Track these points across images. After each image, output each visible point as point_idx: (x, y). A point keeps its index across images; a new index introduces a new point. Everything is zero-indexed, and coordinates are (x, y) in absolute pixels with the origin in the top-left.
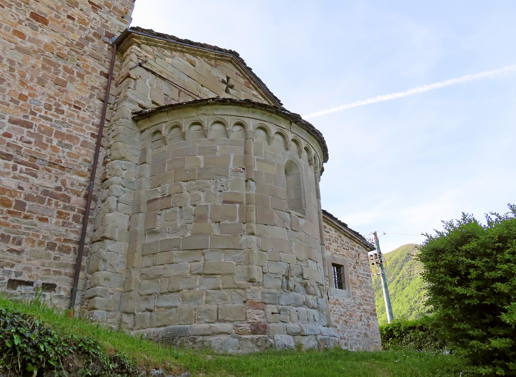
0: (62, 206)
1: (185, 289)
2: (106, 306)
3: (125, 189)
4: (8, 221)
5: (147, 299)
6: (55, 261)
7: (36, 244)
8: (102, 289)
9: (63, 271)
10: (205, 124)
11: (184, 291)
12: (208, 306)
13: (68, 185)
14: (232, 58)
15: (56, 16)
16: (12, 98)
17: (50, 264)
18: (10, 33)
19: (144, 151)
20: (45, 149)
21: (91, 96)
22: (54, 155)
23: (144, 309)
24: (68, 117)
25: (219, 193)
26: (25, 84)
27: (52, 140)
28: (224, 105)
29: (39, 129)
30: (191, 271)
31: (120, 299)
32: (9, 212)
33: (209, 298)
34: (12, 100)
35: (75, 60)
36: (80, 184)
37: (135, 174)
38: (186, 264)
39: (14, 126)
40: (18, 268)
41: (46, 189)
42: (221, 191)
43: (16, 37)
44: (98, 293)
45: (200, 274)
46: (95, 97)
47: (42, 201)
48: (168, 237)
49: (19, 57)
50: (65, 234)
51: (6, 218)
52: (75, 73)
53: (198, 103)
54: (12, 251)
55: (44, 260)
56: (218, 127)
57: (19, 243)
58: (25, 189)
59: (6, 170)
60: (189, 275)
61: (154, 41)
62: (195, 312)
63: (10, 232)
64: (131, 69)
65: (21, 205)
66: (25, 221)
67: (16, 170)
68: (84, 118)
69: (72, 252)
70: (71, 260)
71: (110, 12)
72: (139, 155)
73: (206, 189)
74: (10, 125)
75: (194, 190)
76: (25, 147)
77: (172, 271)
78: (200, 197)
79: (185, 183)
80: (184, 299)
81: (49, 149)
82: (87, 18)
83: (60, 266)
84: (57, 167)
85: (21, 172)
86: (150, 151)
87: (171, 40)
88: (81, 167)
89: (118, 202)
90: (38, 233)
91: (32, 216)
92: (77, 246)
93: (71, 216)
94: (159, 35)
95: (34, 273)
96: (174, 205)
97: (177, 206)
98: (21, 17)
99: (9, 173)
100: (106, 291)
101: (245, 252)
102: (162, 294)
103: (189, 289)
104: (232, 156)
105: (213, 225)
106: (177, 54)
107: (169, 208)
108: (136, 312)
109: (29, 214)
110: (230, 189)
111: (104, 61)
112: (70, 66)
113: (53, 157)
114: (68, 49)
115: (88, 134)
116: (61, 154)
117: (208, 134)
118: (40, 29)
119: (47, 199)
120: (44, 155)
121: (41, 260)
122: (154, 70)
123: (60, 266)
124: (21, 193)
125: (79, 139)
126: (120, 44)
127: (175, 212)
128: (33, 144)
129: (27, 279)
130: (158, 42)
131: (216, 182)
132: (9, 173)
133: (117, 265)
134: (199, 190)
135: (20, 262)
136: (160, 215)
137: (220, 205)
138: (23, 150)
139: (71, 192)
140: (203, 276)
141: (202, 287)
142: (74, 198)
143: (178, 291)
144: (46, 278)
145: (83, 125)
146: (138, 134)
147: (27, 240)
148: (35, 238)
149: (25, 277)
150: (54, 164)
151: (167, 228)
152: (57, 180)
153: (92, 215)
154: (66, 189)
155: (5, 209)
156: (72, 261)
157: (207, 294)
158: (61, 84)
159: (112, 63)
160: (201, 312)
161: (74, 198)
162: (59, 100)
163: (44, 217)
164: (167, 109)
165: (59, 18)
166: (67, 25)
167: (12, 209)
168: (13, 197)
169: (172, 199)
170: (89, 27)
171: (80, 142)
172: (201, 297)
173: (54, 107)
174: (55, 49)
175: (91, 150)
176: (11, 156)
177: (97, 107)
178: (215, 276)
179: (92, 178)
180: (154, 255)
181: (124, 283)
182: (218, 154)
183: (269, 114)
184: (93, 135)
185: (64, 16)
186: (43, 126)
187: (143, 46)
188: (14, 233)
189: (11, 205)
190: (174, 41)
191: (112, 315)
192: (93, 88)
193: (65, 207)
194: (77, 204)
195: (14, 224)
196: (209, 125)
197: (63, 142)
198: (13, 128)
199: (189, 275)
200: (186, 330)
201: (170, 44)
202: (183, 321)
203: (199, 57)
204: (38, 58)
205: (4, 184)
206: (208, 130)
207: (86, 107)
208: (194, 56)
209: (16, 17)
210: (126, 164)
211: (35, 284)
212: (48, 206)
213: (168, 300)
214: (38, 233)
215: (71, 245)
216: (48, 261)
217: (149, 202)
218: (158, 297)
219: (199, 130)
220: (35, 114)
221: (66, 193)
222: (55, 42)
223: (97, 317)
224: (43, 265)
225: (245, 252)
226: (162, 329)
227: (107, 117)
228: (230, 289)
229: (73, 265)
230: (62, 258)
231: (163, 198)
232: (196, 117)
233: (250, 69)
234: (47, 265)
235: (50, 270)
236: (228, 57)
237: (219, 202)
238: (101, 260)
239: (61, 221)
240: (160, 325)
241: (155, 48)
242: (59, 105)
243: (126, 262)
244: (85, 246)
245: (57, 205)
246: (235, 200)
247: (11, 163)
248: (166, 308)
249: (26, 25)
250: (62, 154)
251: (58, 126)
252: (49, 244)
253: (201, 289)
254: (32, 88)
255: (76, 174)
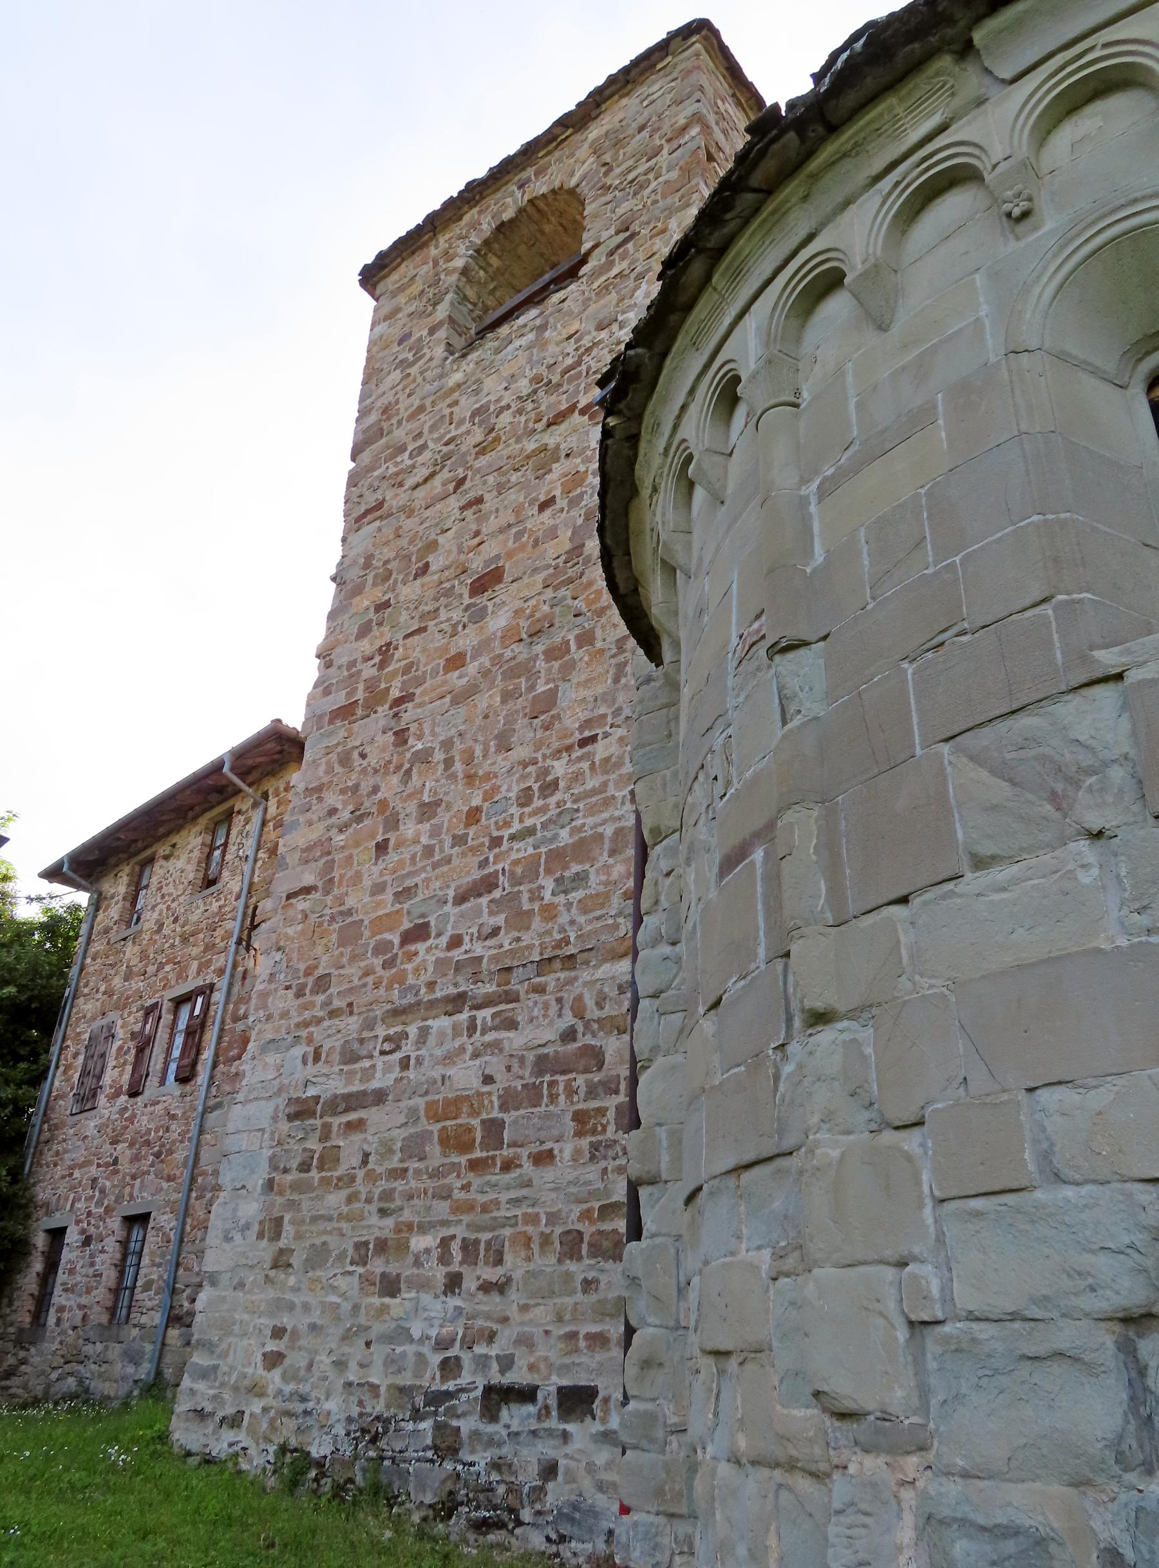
2: (659, 1493)
32: (474, 1165)
50: (600, 1185)
55: (558, 1301)
65: (494, 1128)
115: (623, 803)
121: (551, 1302)
139: (601, 1028)
148: (530, 1229)
149: (518, 1377)
167: (478, 1154)
183: (792, 190)
193: (592, 1093)
216: (569, 1301)
245: (571, 1092)
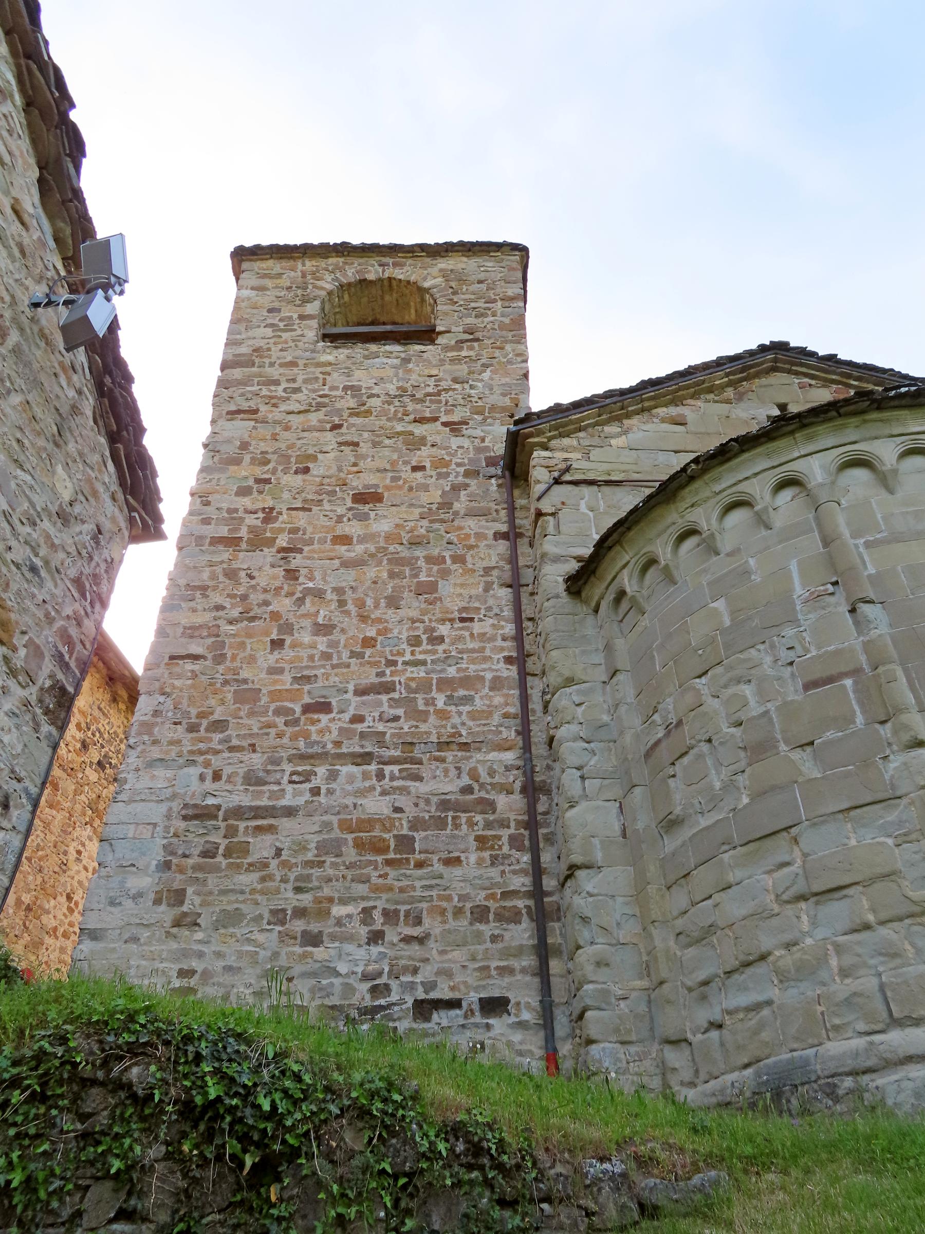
0: (481, 824)
1: (777, 947)
2: (617, 1030)
3: (592, 745)
4: (389, 881)
5: (704, 998)
6: (494, 946)
7: (450, 915)
8: (596, 990)
9: (516, 964)
10: (704, 526)
11: (777, 953)
12: (852, 985)
13: (484, 777)
14: (775, 360)
15: (394, 479)
16: (352, 652)
17: (487, 955)
18: (328, 546)
19: (608, 648)
20: (425, 721)
21: (488, 587)
22: (445, 727)
23: (706, 1025)
24: (453, 644)
25: (789, 669)
26: (368, 617)
27: (434, 699)
28: (729, 460)
29: (408, 687)
30: (777, 896)
31: (650, 1008)
32: (388, 863)
33: (848, 960)
34: (353, 654)
35: (442, 537)
36: (506, 767)
37: (606, 707)
38: (759, 881)
39: (364, 698)
40: (426, 973)
41: (443, 797)
42: (791, 663)
43: (337, 547)
44: (589, 1002)
45: (802, 898)
46: (495, 586)
47: (441, 824)
48: (704, 822)
49: (348, 577)
51: (384, 876)
52: (447, 558)
53: (669, 490)
54: (407, 940)
55: (472, 947)
56: (738, 516)
57: (418, 922)
58: (407, 809)
59: (367, 784)
60: (776, 908)
61: (571, 422)
62: (820, 1009)
63: (397, 903)
64: (539, 499)
65: (405, 843)
66: (420, 872)
67: (384, 777)
68: (484, 634)
69: (525, 918)
70: (527, 935)
71: (485, 420)
72: (603, 661)
73: (753, 671)
74: (358, 699)
75: (726, 686)
76: (389, 730)
77: (733, 907)
78: (745, 697)
79: (704, 680)
80: (784, 978)
81: (432, 719)
82: (447, 454)
83: (507, 953)
84: (454, 747)
85: (392, 778)
86: (620, 644)
87: (608, 401)
88: (501, 732)
89: (582, 778)
90: (448, 892)
91: (430, 860)
92: (531, 903)
93: (505, 839)
94: (577, 405)
95: (458, 978)
96: (693, 742)
97: (700, 741)
98: (340, 510)
99: (373, 788)
100: (605, 993)
101: (912, 803)
102: (729, 973)
103: (788, 946)
104: (794, 567)
105: (796, 755)
106: (634, 421)
107: (686, 753)
108: (689, 1036)
109: (423, 856)
110: (812, 648)
111: (497, 511)
112: (436, 552)
113: (443, 731)
114: (425, 523)
116: (456, 720)
117: (719, 544)
118: (372, 514)
119: (450, 818)
120: (426, 733)
121: (466, 948)
122: (591, 476)
123: (507, 953)
124: (400, 819)
125: (483, 678)
126: (514, 467)
127: (700, 756)
128: (402, 720)
129: (447, 995)
130: (582, 420)
131: (773, 646)
132: (373, 788)
133: (618, 924)
134: (739, 682)
135: (428, 959)
136: (674, 776)
137: (799, 698)
138: (388, 735)
139: (493, 789)
140: (813, 899)
141: (820, 933)
142: (502, 801)
143: (763, 957)
144: (484, 987)
145: (484, 648)
146: (590, 620)
147: (431, 911)
148: (444, 904)
149: (443, 992)
150: (448, 743)
151: (696, 802)
152: (459, 774)
153: (548, 825)
154: (482, 786)
155: (380, 859)
156: (529, 937)
157: (839, 949)
158: (427, 590)
159: (512, 509)
160: (837, 1005)
161: (502, 801)
162: (430, 620)
163: (451, 855)
164: (615, 536)
165: (399, 478)
166: (414, 484)
167: (391, 856)
168: (389, 831)
169: (686, 728)
170: (453, 466)
171: (487, 684)
172: (823, 960)
173: (424, 637)
174: (403, 534)
175: (512, 692)
176: (369, 754)
177: (504, 602)
178: (845, 892)
179: (527, 747)
180: (689, 878)
181: (647, 966)
182: (756, 578)
183: (854, 420)
184: (509, 660)
185: (406, 473)
186: (413, 679)
187: (553, 443)
188: (403, 903)
189: (389, 847)
190: (614, 399)
191: (637, 1053)
192: (487, 570)
193: (488, 825)
194: (511, 810)
195: (401, 884)
196: (714, 522)
197: (456, 694)
198: (364, 703)
199: (776, 908)
200: (806, 1062)
201: (608, 409)
202: (797, 1039)
203: (690, 401)
204: (379, 563)
205: (368, 811)
206: (712, 535)
207: (483, 612)
208: (677, 405)
209: (331, 514)
210: (578, 692)
211: (464, 1004)
212: (456, 832)
213: (746, 989)
214: (448, 892)
215: (520, 903)
217: (648, 755)
218: (723, 984)
219: (698, 545)
220: (394, 663)
221: (483, 794)
222: (401, 522)
223: (600, 1061)
224: (474, 959)
225: (912, 803)
226: (749, 1072)
227: (527, 612)
228: (900, 919)
229: (533, 946)
230: (507, 935)
231: (668, 734)
232: (680, 521)
233: (832, 358)
234: (479, 957)
235: (488, 967)
236: (762, 363)
237: (793, 693)
238: (578, 920)
239: (486, 854)
240: (746, 1061)
241: (582, 434)
242: (433, 630)
243: (638, 914)
244: (546, 900)
245: (471, 824)
246: (834, 671)
247: (373, 767)
248: (749, 1009)
249: (349, 520)
250: (461, 721)
251: (439, 668)
252: (475, 910)
253: (820, 937)
254: (379, 620)
255: (494, 750)
